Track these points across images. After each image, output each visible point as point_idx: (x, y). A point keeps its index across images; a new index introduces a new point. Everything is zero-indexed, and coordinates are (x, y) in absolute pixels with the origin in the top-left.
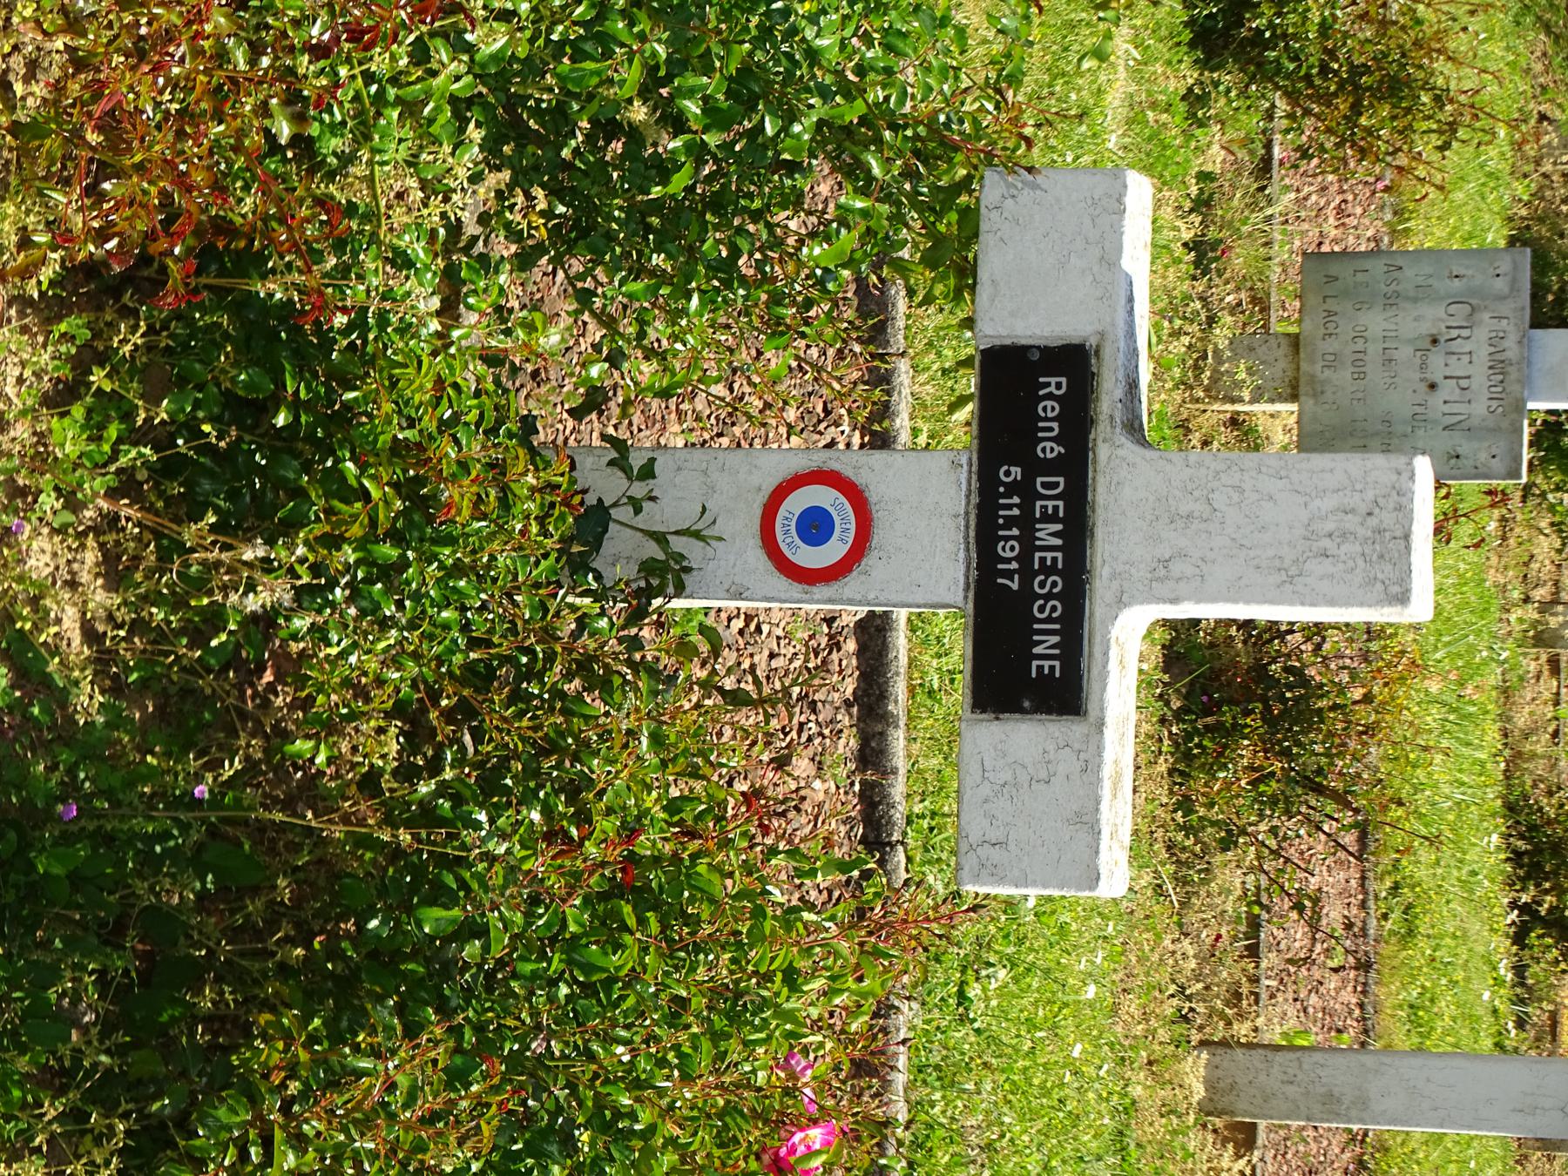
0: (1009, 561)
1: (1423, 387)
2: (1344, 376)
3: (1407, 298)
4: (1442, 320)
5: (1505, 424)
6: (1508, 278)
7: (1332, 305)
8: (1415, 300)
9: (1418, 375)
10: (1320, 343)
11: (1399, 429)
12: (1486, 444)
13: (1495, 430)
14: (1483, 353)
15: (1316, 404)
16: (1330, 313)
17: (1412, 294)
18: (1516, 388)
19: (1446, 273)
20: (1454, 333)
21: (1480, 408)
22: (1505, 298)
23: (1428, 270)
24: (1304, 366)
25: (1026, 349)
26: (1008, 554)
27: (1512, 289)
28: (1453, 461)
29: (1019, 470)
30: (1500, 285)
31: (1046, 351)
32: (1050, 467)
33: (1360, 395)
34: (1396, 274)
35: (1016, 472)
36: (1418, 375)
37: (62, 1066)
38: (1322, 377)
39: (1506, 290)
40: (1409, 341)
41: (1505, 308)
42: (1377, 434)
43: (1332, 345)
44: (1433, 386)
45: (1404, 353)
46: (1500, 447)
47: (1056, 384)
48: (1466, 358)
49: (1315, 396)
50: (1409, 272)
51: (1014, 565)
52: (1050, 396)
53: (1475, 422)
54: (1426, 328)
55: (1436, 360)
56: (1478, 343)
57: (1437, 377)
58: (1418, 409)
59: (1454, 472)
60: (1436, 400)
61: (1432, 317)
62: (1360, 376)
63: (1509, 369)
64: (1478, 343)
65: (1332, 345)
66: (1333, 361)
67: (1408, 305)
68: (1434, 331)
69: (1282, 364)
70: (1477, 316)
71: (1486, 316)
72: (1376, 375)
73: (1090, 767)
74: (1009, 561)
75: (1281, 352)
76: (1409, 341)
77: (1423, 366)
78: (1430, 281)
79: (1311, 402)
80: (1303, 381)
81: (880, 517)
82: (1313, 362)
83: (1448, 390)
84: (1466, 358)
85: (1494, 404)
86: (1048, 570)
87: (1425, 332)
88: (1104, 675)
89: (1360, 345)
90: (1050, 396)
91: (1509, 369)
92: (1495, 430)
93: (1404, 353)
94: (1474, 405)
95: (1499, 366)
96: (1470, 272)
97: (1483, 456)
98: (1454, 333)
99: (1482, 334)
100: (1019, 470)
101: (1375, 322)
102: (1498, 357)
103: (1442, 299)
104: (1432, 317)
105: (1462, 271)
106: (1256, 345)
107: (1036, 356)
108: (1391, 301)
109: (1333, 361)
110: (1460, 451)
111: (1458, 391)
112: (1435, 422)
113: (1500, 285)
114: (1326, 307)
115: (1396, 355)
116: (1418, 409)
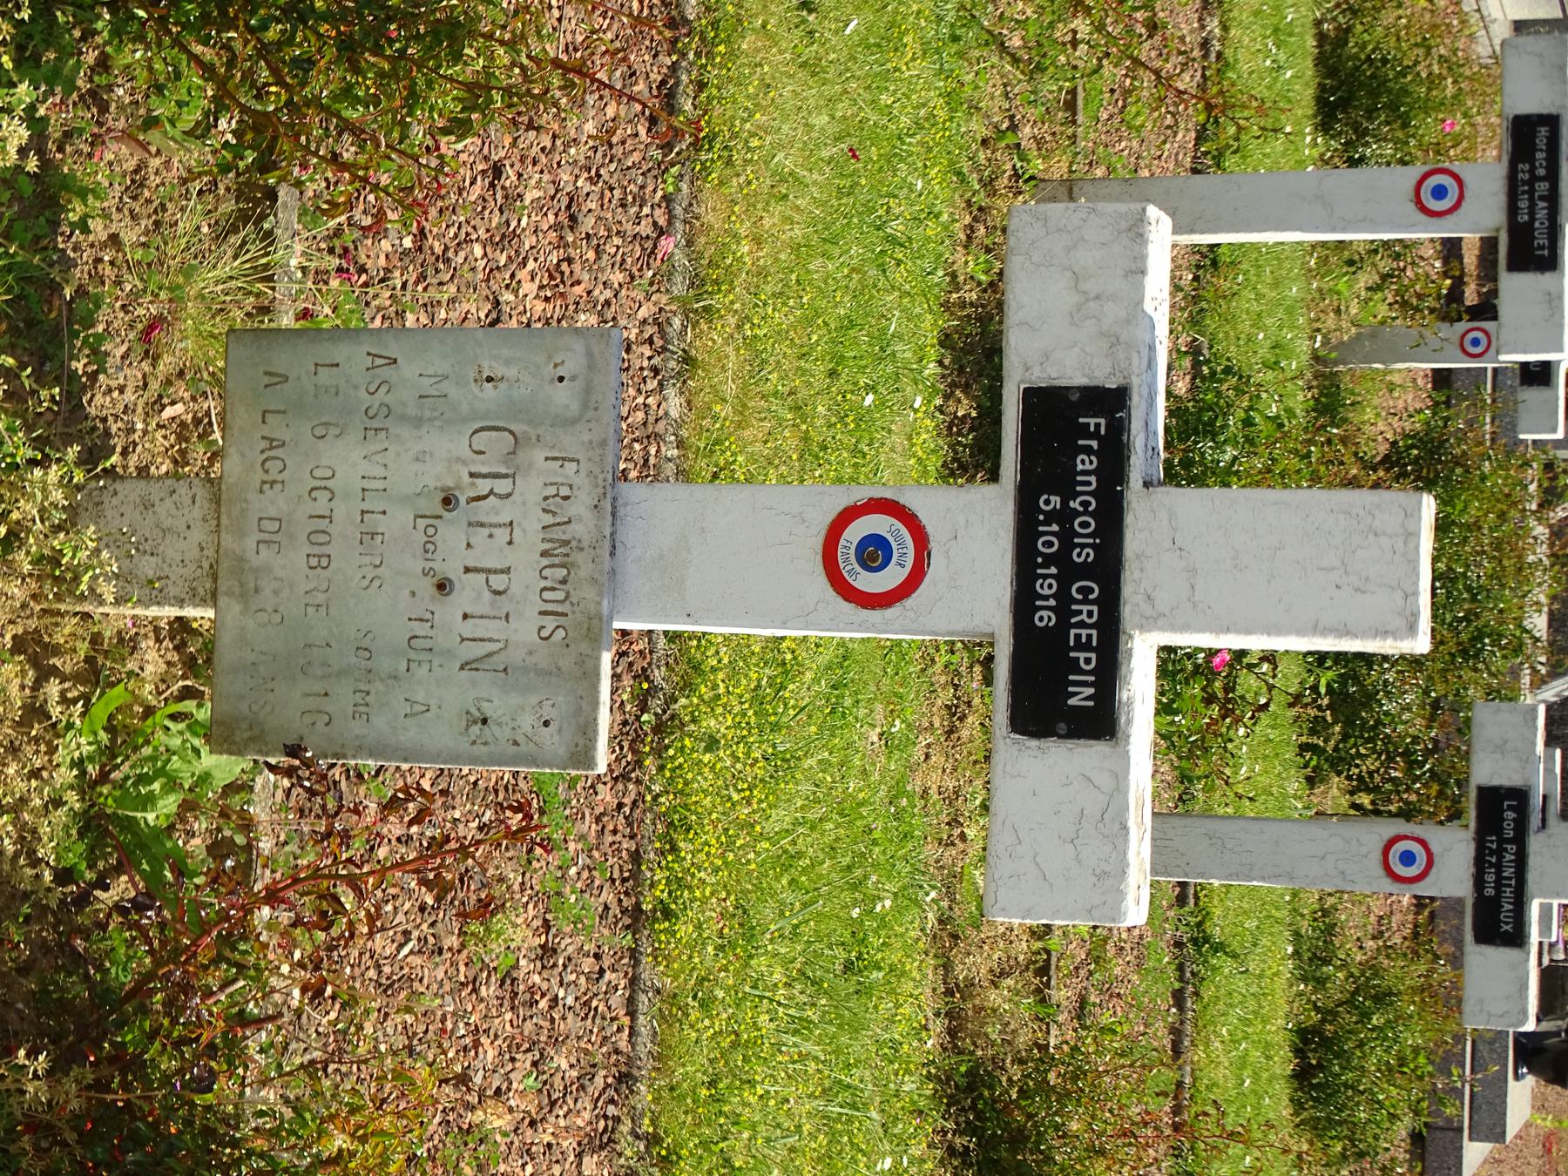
0: (1046, 598)
1: (427, 587)
2: (292, 561)
3: (404, 418)
4: (464, 462)
5: (567, 663)
6: (579, 384)
7: (276, 427)
8: (418, 422)
9: (419, 565)
10: (253, 496)
11: (384, 664)
12: (534, 700)
13: (549, 674)
14: (532, 524)
15: (245, 611)
16: (272, 443)
17: (412, 411)
18: (589, 593)
19: (472, 375)
20: (484, 486)
21: (525, 629)
22: (574, 422)
23: (441, 366)
24: (227, 540)
25: (1071, 735)
26: (1046, 592)
27: (585, 406)
28: (476, 729)
29: (1058, 499)
30: (564, 398)
31: (1087, 391)
32: (1085, 571)
33: (320, 598)
34: (386, 373)
35: (1056, 501)
36: (419, 565)
37: (123, 1075)
38: (256, 561)
39: (575, 407)
40: (406, 499)
41: (571, 442)
42: (344, 672)
43: (273, 503)
44: (443, 586)
45: (397, 521)
46: (558, 705)
47: (1543, 131)
48: (502, 535)
49: (243, 596)
50: (408, 370)
51: (1052, 602)
52: (1082, 625)
53: (516, 656)
54: (435, 475)
55: (452, 534)
56: (524, 507)
57: (453, 570)
58: (420, 629)
59: (480, 750)
60: (449, 612)
61: (443, 456)
62: (320, 562)
63: (579, 558)
64: (524, 507)
65: (273, 503)
66: (275, 534)
67: (405, 431)
68: (450, 483)
69: (198, 534)
70: (522, 454)
71: (539, 455)
72: (348, 562)
73: (1120, 777)
74: (1046, 598)
75: (197, 512)
76: (406, 499)
77: (429, 547)
78: (445, 387)
79: (236, 608)
80: (225, 565)
81: (1381, 872)
82: (241, 534)
83: (470, 591)
84: (502, 535)
85: (550, 623)
86: (1492, 852)
87: (432, 484)
88: (1129, 722)
89: (321, 506)
90: (1082, 625)
91: (579, 558)
92: (549, 674)
93: (397, 521)
94: (513, 623)
95: (559, 551)
96: (512, 373)
97: (527, 722)
98: (484, 486)
99: (531, 489)
100: (1058, 499)
101: (348, 460)
102: (557, 533)
103: (464, 420)
104: (443, 456)
105: (499, 371)
106: (155, 498)
107: (1062, 728)
108: (377, 422)
109: (275, 534)
110: (488, 710)
111: (487, 594)
112: (448, 653)
113: (564, 398)
114: (266, 431)
115: (382, 524)
116: (420, 629)
